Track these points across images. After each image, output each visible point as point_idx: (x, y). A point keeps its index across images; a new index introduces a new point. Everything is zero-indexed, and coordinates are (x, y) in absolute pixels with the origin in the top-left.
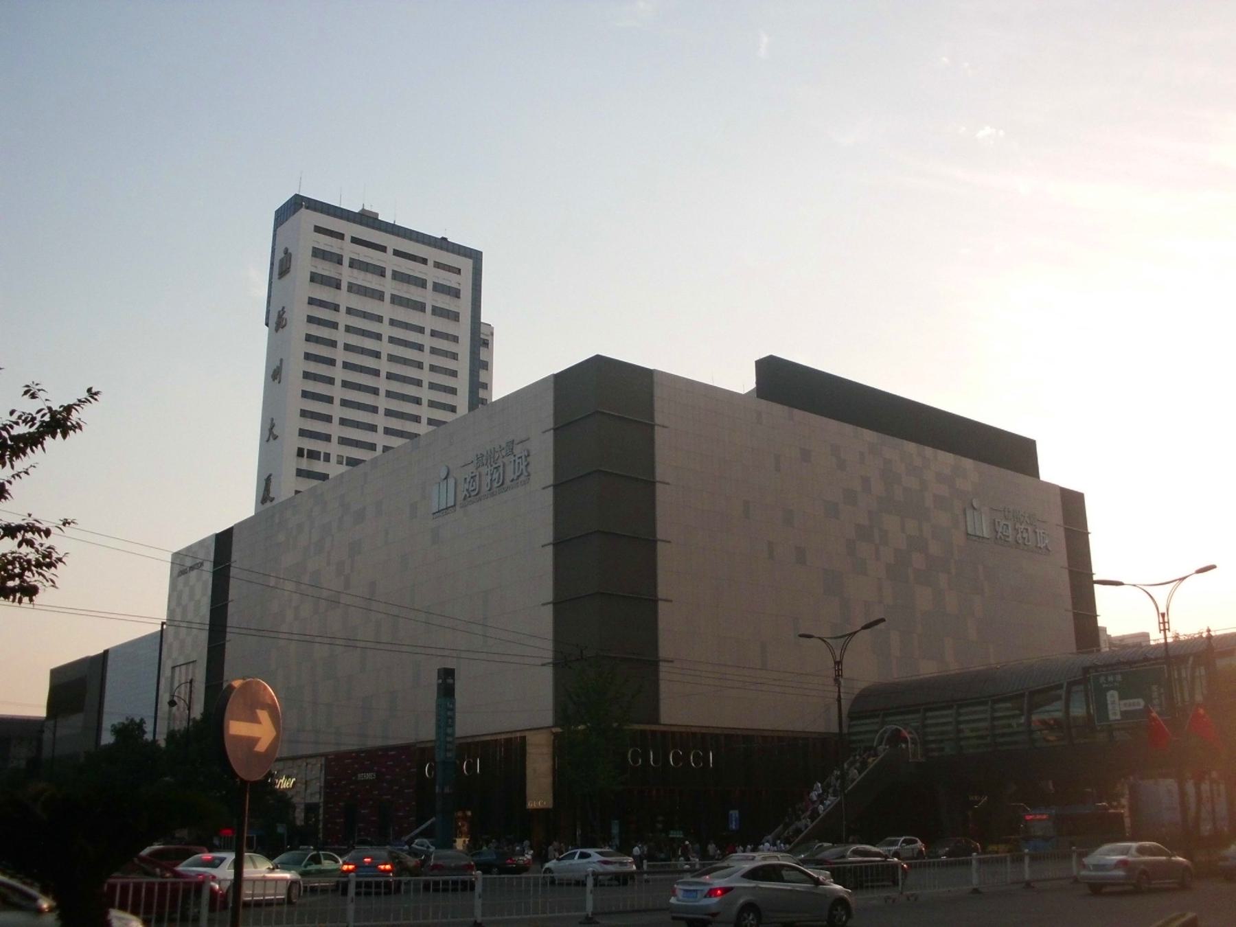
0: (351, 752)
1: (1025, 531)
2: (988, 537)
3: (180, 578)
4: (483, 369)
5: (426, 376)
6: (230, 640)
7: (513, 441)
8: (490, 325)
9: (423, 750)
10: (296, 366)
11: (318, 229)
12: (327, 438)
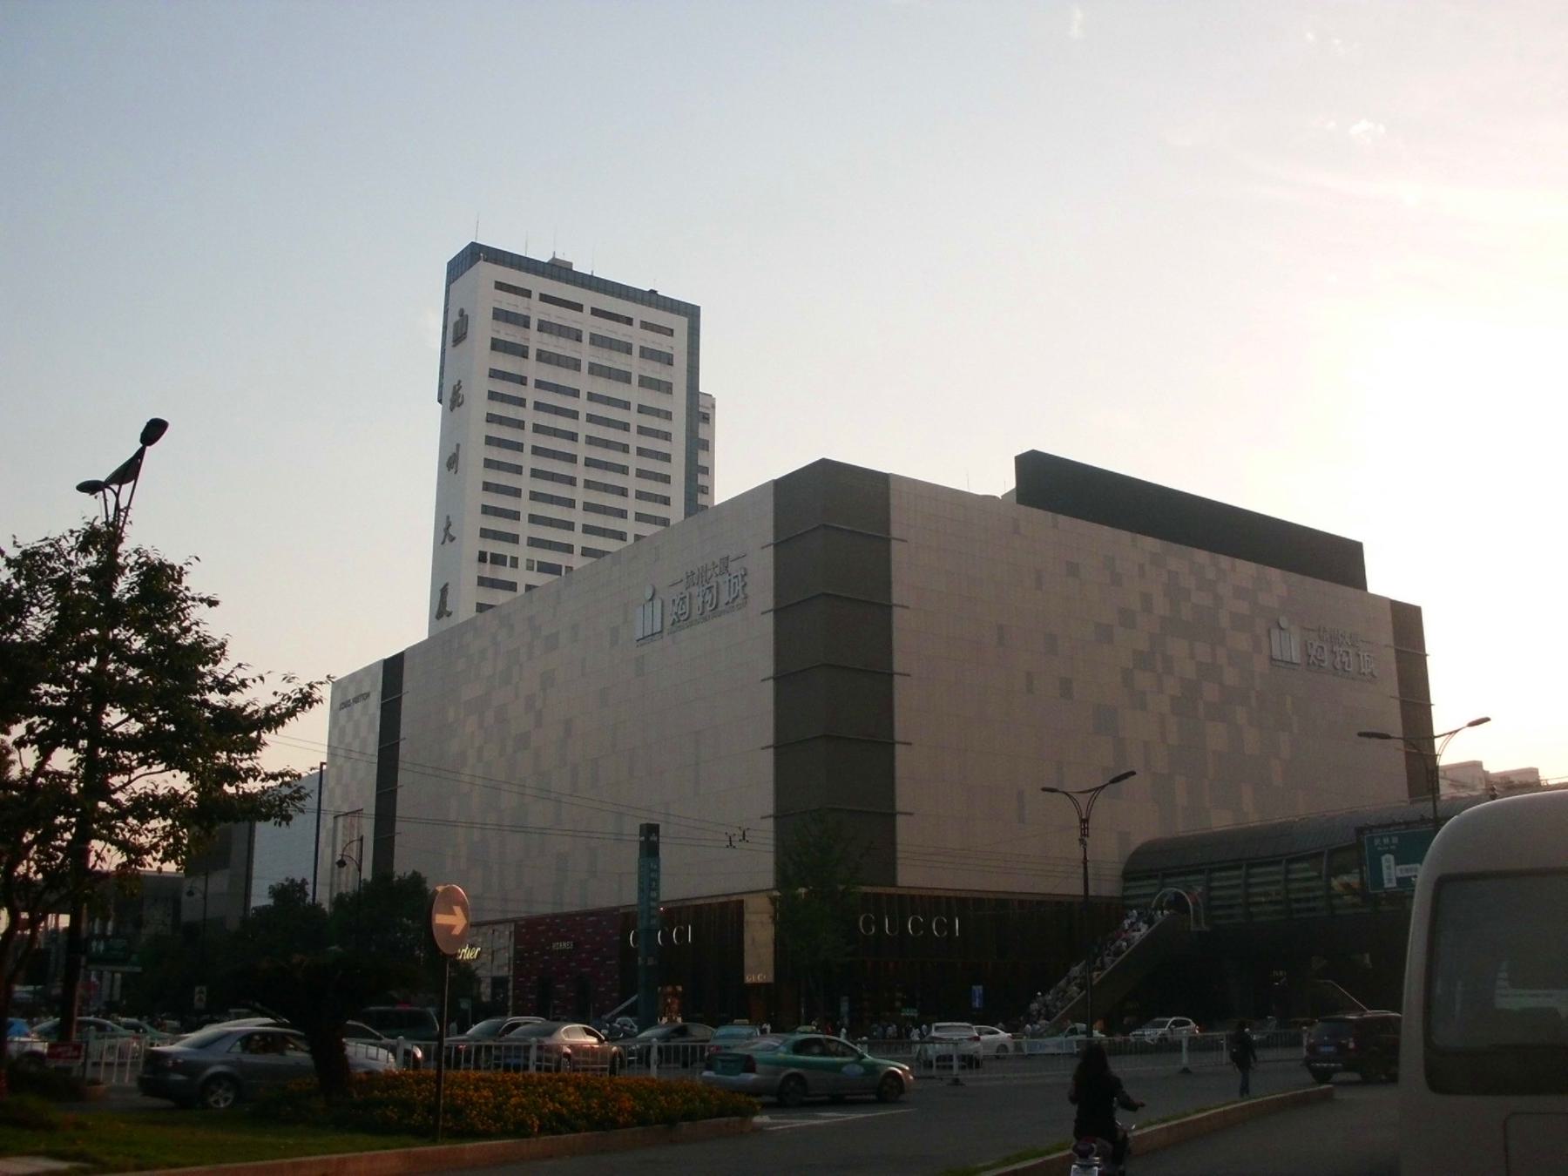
1: (1344, 654)
2: (1299, 662)
3: (342, 711)
4: (703, 449)
5: (633, 461)
7: (727, 558)
8: (711, 396)
9: (626, 915)
10: (476, 451)
11: (500, 286)
12: (514, 539)
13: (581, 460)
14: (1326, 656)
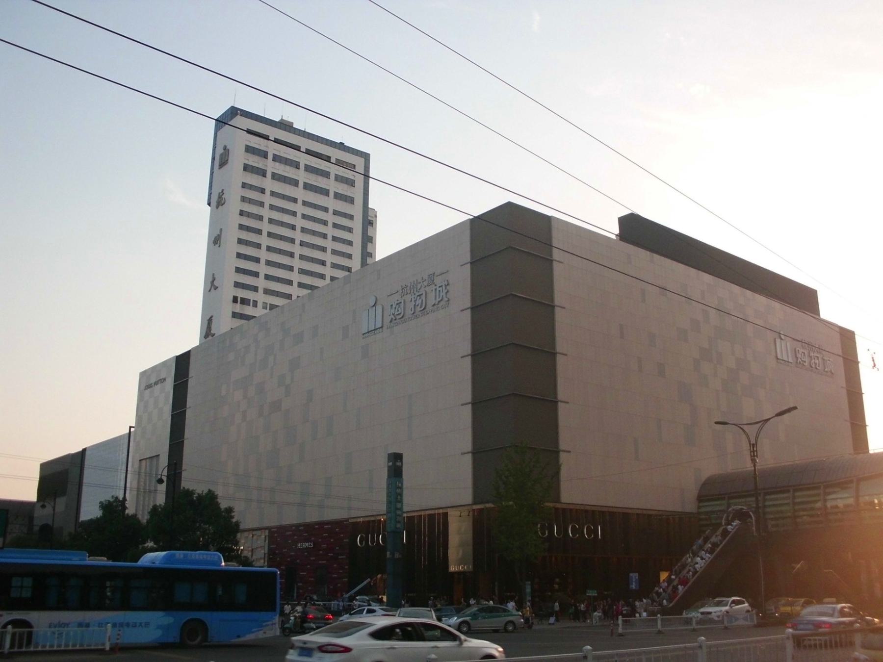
0: (291, 526)
2: (792, 362)
3: (146, 391)
6: (188, 439)
7: (434, 273)
8: (374, 210)
10: (232, 235)
12: (255, 289)
13: (297, 242)
14: (807, 359)
